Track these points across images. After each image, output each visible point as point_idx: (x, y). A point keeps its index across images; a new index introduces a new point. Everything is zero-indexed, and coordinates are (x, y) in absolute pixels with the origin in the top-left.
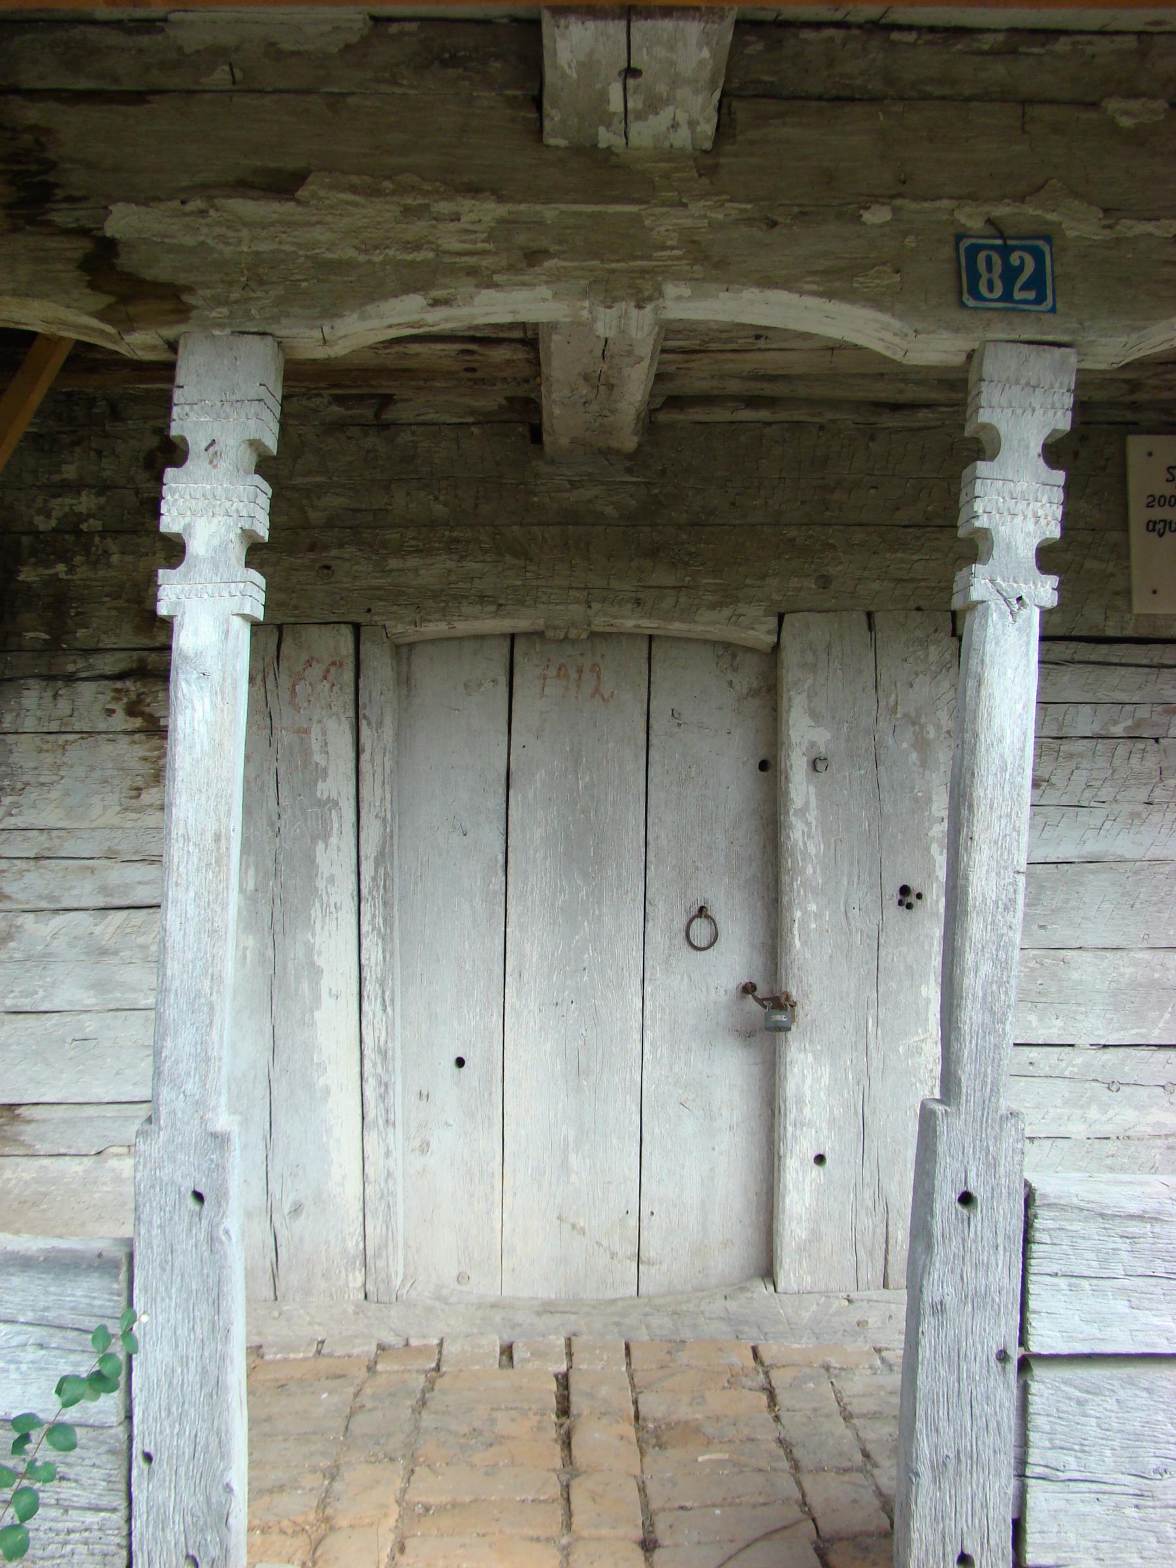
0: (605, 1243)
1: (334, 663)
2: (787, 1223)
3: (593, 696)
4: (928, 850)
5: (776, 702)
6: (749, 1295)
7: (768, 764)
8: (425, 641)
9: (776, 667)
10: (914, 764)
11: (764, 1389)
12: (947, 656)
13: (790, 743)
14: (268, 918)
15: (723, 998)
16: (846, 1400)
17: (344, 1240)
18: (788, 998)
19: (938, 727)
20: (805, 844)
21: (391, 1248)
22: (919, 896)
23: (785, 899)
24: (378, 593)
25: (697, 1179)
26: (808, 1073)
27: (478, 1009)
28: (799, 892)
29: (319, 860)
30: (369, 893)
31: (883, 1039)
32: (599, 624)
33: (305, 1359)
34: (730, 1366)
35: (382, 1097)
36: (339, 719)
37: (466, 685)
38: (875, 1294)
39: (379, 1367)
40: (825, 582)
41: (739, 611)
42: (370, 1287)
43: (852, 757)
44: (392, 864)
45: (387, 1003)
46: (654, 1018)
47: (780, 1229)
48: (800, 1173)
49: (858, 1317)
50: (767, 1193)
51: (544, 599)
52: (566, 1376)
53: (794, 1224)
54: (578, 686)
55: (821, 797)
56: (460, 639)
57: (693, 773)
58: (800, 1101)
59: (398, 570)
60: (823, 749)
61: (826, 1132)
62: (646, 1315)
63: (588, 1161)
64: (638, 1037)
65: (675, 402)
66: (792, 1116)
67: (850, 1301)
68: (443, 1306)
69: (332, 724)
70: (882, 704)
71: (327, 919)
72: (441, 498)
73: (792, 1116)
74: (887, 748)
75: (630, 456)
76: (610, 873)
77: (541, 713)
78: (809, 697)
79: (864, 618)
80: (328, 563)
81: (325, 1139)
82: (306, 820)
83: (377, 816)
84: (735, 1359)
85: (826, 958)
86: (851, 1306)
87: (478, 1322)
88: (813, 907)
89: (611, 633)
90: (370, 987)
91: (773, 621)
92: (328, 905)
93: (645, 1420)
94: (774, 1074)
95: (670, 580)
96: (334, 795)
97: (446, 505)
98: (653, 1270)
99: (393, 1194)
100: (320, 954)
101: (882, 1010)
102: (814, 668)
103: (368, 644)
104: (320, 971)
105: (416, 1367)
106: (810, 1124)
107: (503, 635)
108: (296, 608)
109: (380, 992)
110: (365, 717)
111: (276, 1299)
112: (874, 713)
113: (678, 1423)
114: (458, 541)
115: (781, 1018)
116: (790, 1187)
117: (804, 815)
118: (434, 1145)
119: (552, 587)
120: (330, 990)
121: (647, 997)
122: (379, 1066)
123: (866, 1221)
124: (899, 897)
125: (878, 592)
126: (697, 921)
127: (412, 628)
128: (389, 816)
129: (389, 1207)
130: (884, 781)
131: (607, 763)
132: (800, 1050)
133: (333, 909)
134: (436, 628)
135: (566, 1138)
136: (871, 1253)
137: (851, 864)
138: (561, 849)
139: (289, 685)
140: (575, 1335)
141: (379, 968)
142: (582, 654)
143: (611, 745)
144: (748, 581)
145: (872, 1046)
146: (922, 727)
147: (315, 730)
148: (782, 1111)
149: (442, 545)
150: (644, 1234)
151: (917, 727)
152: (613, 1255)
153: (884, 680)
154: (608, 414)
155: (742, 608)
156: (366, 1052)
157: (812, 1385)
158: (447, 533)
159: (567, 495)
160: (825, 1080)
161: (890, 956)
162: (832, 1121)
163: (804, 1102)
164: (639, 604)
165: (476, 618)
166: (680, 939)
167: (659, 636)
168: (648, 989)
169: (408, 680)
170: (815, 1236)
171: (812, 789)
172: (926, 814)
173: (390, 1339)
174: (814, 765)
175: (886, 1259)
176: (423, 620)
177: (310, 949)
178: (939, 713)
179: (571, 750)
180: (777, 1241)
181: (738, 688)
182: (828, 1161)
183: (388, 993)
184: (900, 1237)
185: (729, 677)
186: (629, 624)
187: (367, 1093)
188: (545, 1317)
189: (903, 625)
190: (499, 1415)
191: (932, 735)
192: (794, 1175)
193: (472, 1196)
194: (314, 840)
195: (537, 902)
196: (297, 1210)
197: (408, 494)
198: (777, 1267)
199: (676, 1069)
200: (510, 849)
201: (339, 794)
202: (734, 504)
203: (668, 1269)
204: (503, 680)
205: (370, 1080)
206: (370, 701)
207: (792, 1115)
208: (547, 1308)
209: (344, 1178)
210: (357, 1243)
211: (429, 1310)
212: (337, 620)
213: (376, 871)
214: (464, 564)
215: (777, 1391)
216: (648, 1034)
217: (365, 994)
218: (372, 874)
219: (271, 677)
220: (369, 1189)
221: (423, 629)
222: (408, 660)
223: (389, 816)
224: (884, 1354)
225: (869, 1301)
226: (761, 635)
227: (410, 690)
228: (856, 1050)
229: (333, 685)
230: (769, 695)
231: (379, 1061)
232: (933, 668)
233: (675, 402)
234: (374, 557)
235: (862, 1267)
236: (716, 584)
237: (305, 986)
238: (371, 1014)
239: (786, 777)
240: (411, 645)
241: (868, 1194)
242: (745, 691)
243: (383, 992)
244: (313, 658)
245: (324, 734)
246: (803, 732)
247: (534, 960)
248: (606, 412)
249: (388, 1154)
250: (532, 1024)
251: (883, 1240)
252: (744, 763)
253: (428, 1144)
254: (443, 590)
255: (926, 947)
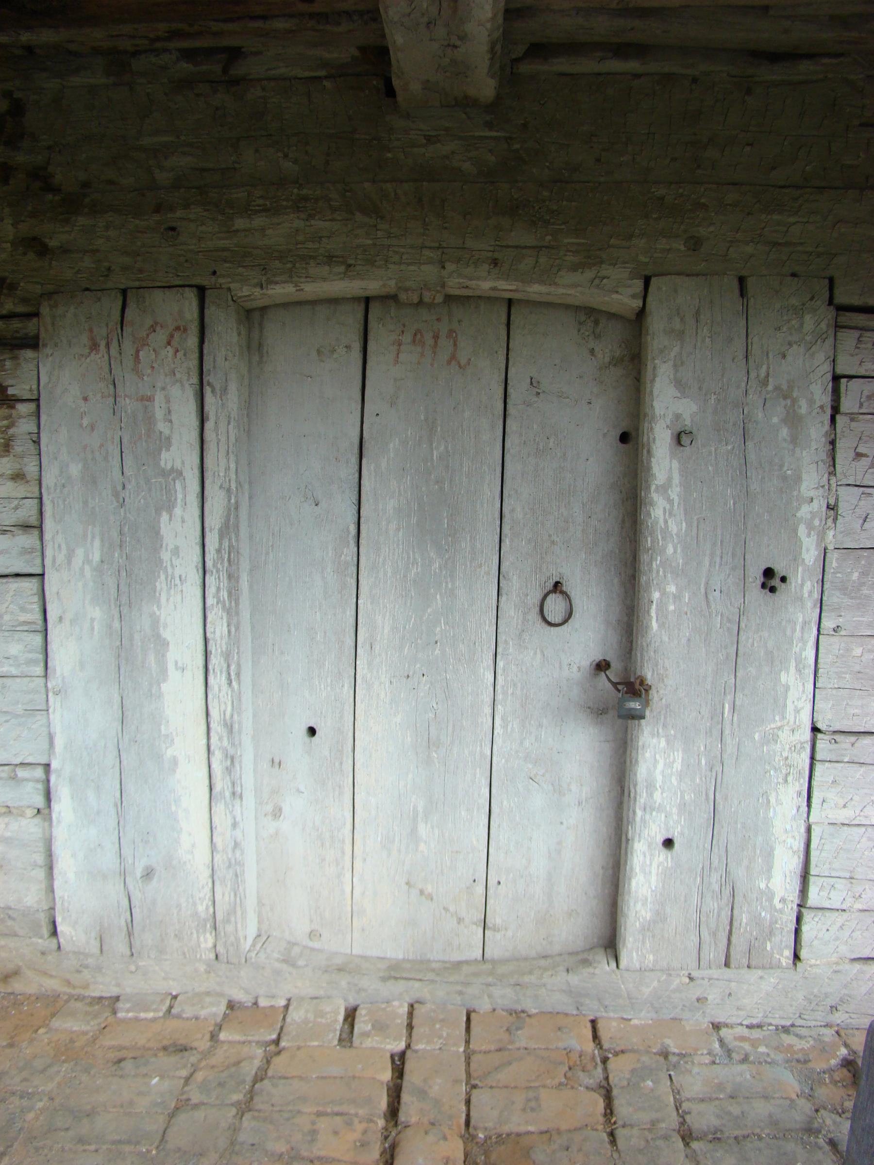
0: (452, 909)
1: (178, 328)
2: (632, 904)
3: (449, 363)
4: (795, 531)
5: (639, 373)
6: (591, 970)
7: (629, 438)
8: (277, 306)
9: (640, 334)
10: (785, 440)
11: (601, 1087)
12: (823, 326)
13: (653, 417)
14: (113, 592)
15: (576, 675)
16: (685, 1106)
17: (194, 904)
18: (642, 682)
19: (811, 402)
20: (666, 522)
21: (239, 913)
22: (783, 579)
23: (643, 579)
24: (225, 254)
25: (542, 854)
26: (661, 759)
27: (329, 681)
28: (658, 572)
29: (163, 531)
30: (214, 566)
31: (739, 726)
32: (454, 286)
33: (154, 1020)
34: (569, 1052)
35: (229, 770)
36: (182, 385)
37: (319, 352)
38: (715, 973)
39: (223, 1036)
40: (695, 244)
41: (604, 273)
42: (221, 949)
43: (718, 431)
44: (237, 536)
45: (233, 677)
46: (505, 693)
47: (625, 909)
48: (648, 857)
49: (698, 993)
50: (613, 868)
51: (396, 258)
52: (402, 1055)
53: (639, 906)
54: (434, 353)
55: (683, 472)
56: (314, 303)
57: (551, 445)
58: (651, 786)
59: (245, 230)
60: (688, 422)
61: (675, 817)
62: (488, 985)
63: (436, 831)
64: (488, 710)
65: (539, 50)
66: (642, 801)
67: (691, 979)
68: (290, 969)
69: (175, 391)
70: (753, 375)
71: (172, 592)
72: (291, 155)
73: (642, 801)
74: (756, 422)
75: (492, 107)
76: (463, 545)
77: (395, 380)
78: (675, 366)
79: (735, 284)
80: (173, 224)
81: (174, 808)
82: (150, 490)
83: (221, 487)
84: (574, 1043)
85: (684, 641)
86: (692, 984)
87: (324, 985)
88: (672, 589)
89: (468, 297)
90: (214, 661)
91: (639, 284)
92: (173, 577)
93: (475, 1128)
94: (625, 752)
95: (529, 239)
96: (178, 465)
97: (295, 162)
98: (498, 936)
99: (241, 864)
100: (165, 626)
101: (739, 695)
102: (681, 335)
103: (213, 308)
104: (165, 644)
105: (256, 1038)
106: (660, 809)
107: (355, 299)
108: (141, 271)
109: (225, 666)
110: (209, 384)
111: (132, 955)
112: (743, 385)
113: (508, 1135)
114: (306, 198)
115: (635, 705)
116: (637, 869)
117: (666, 491)
118: (286, 809)
119: (403, 247)
120: (176, 663)
121: (499, 671)
122: (225, 739)
123: (712, 904)
124: (762, 579)
125: (751, 256)
126: (552, 597)
127: (257, 291)
128: (233, 486)
129: (237, 876)
130: (752, 457)
131: (463, 432)
132: (653, 735)
133: (178, 581)
134: (282, 291)
135: (415, 807)
136: (714, 934)
137: (714, 544)
138: (414, 520)
139: (133, 352)
140: (417, 1002)
141: (224, 642)
142: (438, 320)
143: (467, 414)
144: (613, 241)
145: (727, 732)
146: (794, 401)
147: (159, 397)
148: (632, 795)
149: (290, 203)
150: (490, 902)
151: (789, 402)
152: (460, 920)
153: (755, 350)
154: (458, 43)
155: (606, 270)
156: (212, 725)
157: (649, 1083)
158: (295, 191)
159: (423, 150)
160: (678, 766)
161: (750, 641)
162: (683, 807)
163: (655, 786)
164: (496, 264)
165: (324, 279)
166: (534, 615)
167: (519, 301)
168: (500, 664)
169: (260, 345)
170: (660, 917)
171: (675, 464)
172: (795, 493)
173: (239, 996)
174: (678, 439)
175: (729, 940)
176: (270, 282)
177: (155, 622)
178: (813, 387)
179: (426, 420)
180: (621, 920)
181: (600, 356)
182: (676, 845)
183: (233, 667)
184: (744, 920)
185: (592, 344)
186: (485, 286)
187: (215, 765)
188: (389, 983)
189: (777, 292)
190: (323, 1124)
191: (803, 411)
192: (641, 858)
193: (323, 860)
194: (158, 511)
195: (389, 574)
196: (148, 874)
197: (257, 151)
198: (620, 946)
199: (527, 744)
200: (362, 520)
201: (183, 463)
202: (598, 160)
203: (513, 936)
204: (357, 347)
205: (217, 752)
206: (214, 367)
207: (642, 800)
208: (394, 971)
209: (193, 846)
210: (207, 908)
211: (277, 972)
212: (181, 283)
213: (221, 544)
214: (313, 222)
215: (615, 1092)
216: (499, 708)
217: (210, 667)
218: (217, 546)
219: (115, 344)
220: (217, 857)
221: (270, 292)
222: (261, 325)
223: (233, 486)
224: (724, 1032)
225: (710, 979)
226: (625, 300)
227: (261, 357)
228: (711, 736)
229: (177, 351)
230: (633, 365)
231: (225, 734)
232: (808, 338)
233: (539, 50)
234: (220, 217)
235: (705, 948)
236: (578, 244)
237: (152, 658)
238: (216, 688)
239: (649, 452)
240: (264, 309)
241: (715, 877)
242: (607, 360)
243: (229, 666)
244: (156, 323)
245: (168, 401)
246: (668, 403)
247: (386, 631)
248: (455, 41)
249: (235, 825)
250: (382, 695)
251: (727, 922)
252: (605, 435)
253: (280, 810)
254: (290, 250)
255: (788, 633)
